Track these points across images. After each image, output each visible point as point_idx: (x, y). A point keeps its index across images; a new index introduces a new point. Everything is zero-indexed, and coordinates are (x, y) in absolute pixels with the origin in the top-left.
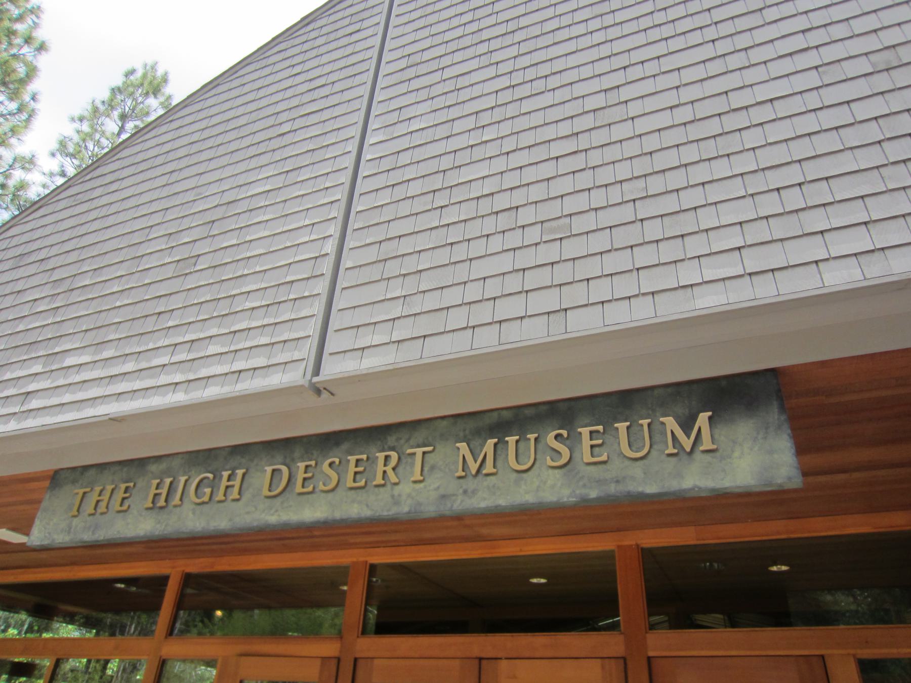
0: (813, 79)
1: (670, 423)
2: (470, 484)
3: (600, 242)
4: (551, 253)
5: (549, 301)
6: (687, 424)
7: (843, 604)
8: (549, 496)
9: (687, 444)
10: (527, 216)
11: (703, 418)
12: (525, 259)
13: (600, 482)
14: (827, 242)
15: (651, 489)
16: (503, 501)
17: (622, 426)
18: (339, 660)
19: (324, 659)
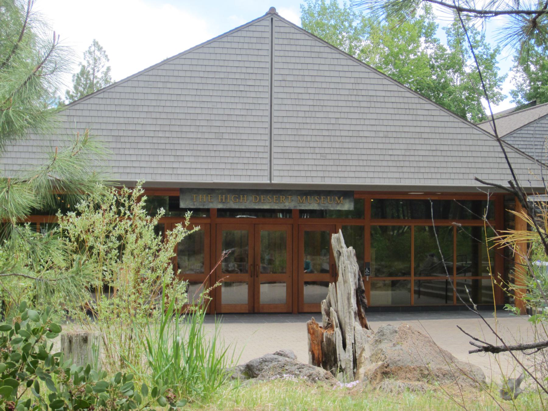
0: (373, 134)
1: (337, 198)
2: (301, 205)
3: (331, 163)
4: (322, 162)
5: (321, 174)
6: (339, 198)
7: (540, 74)
8: (315, 208)
9: (339, 202)
10: (317, 151)
11: (342, 198)
12: (317, 162)
13: (324, 207)
14: (309, 311)
15: (332, 209)
16: (307, 208)
17: (329, 197)
18: (210, 224)
19: (206, 224)
